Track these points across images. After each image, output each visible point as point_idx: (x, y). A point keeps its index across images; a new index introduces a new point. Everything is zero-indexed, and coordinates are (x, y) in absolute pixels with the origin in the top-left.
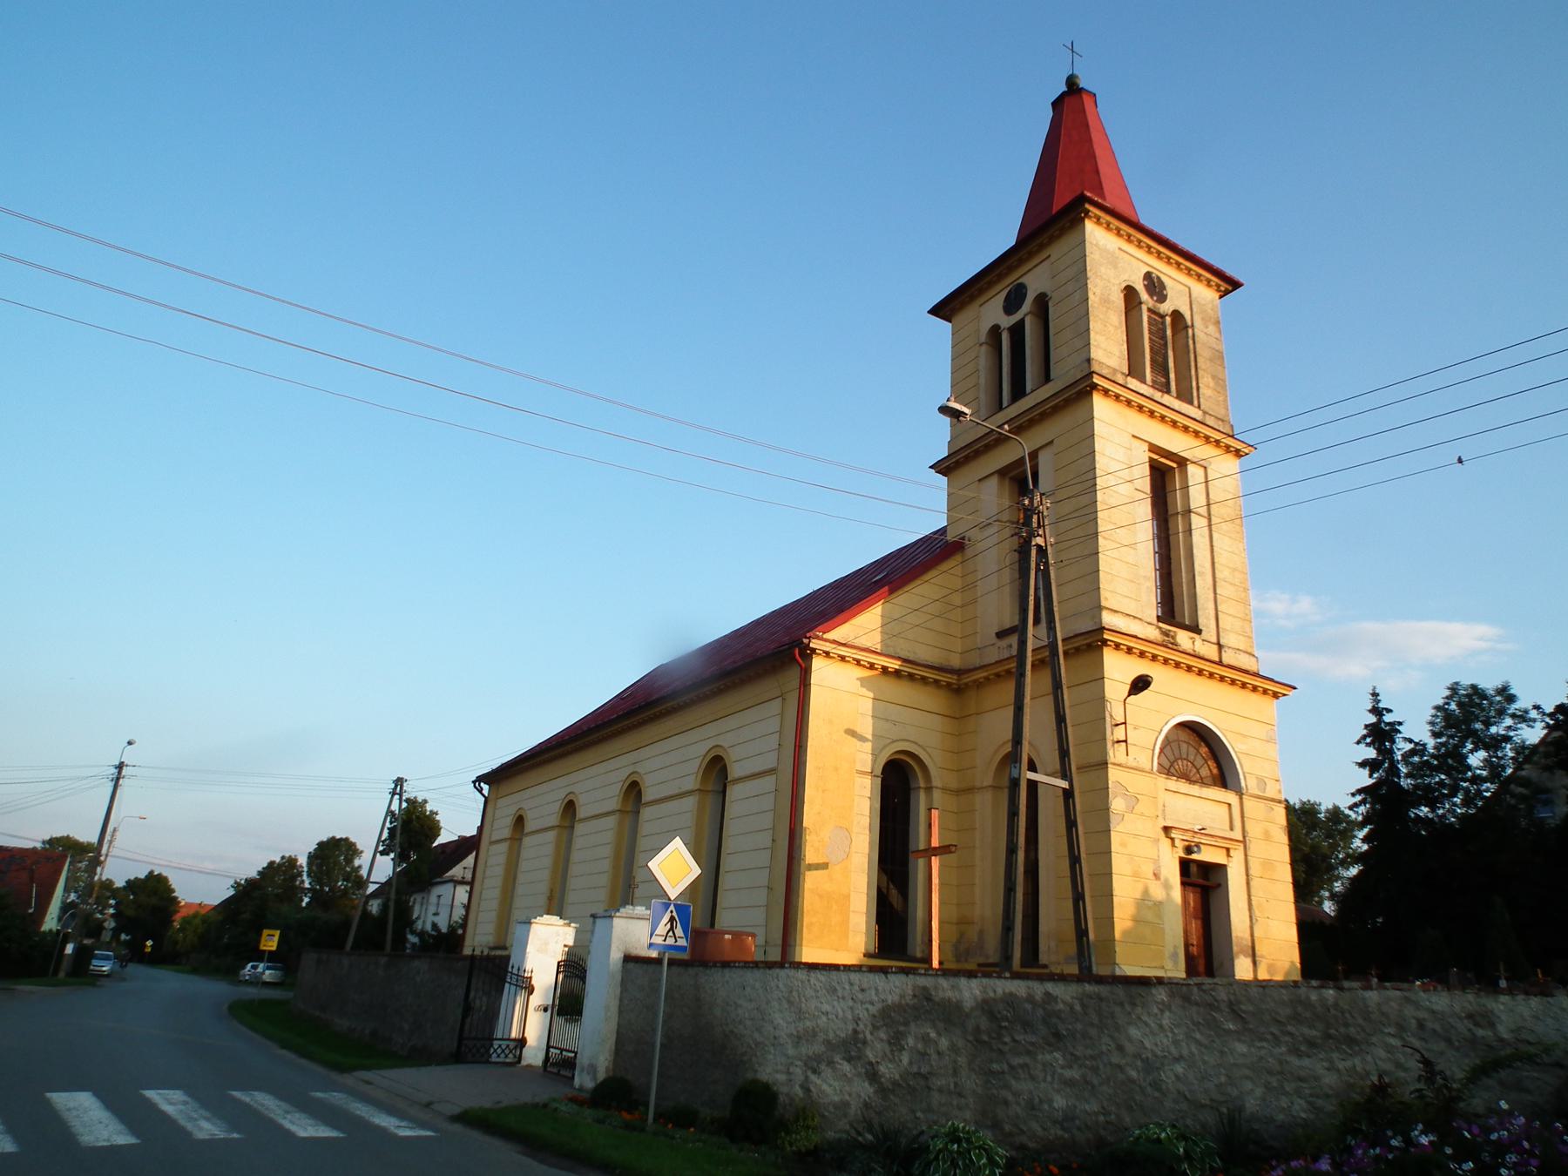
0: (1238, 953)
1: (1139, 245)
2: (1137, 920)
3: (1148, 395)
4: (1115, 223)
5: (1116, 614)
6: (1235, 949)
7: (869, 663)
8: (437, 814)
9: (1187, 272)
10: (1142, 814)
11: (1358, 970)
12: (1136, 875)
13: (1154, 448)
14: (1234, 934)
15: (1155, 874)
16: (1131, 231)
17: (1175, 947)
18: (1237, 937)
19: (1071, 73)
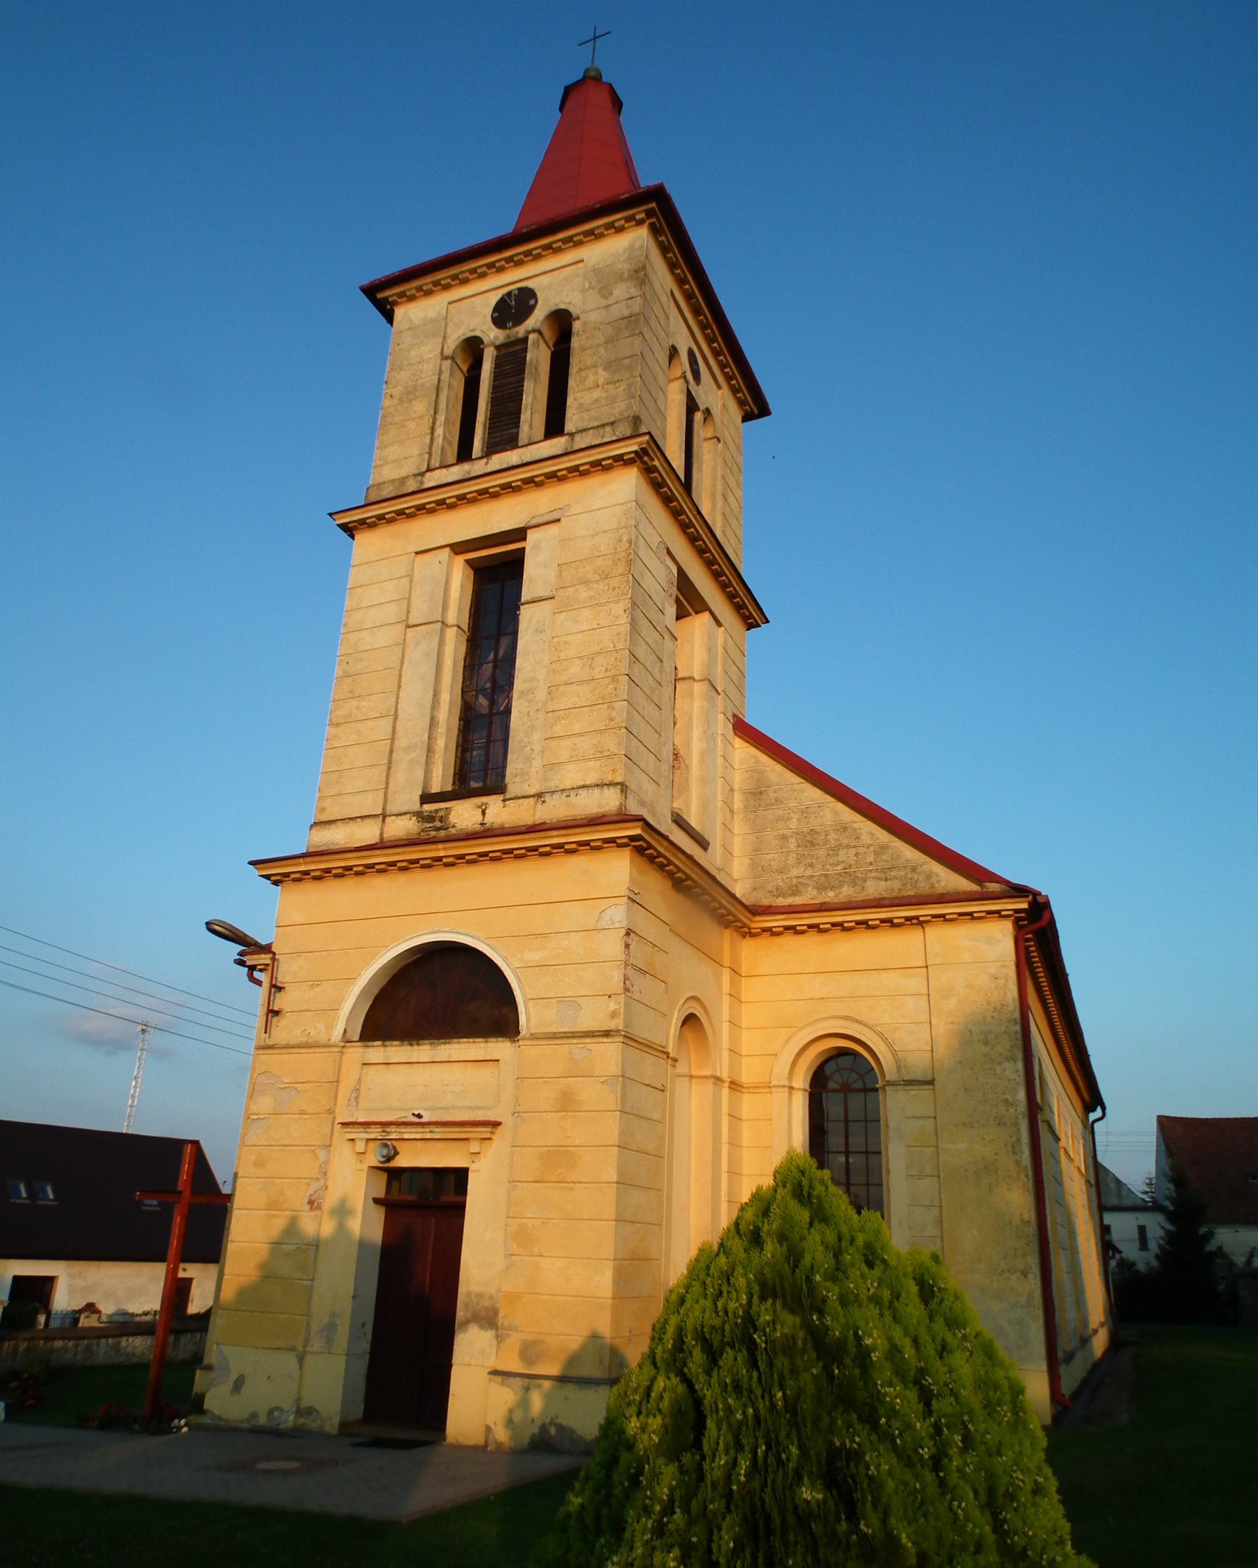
0: (466, 1323)
1: (595, 236)
2: (268, 1274)
3: (560, 452)
4: (426, 281)
5: (333, 826)
6: (460, 1314)
7: (612, 1036)
8: (557, 1417)
9: (512, 264)
10: (302, 1113)
11: (166, 1254)
12: (273, 1206)
13: (458, 548)
14: (462, 1290)
15: (311, 1202)
16: (454, 270)
17: (333, 1315)
18: (469, 1293)
19: (589, 65)
